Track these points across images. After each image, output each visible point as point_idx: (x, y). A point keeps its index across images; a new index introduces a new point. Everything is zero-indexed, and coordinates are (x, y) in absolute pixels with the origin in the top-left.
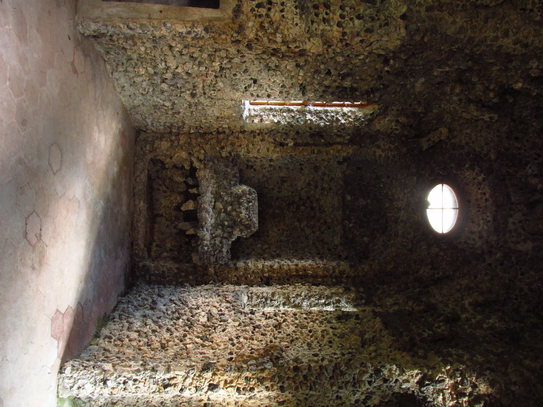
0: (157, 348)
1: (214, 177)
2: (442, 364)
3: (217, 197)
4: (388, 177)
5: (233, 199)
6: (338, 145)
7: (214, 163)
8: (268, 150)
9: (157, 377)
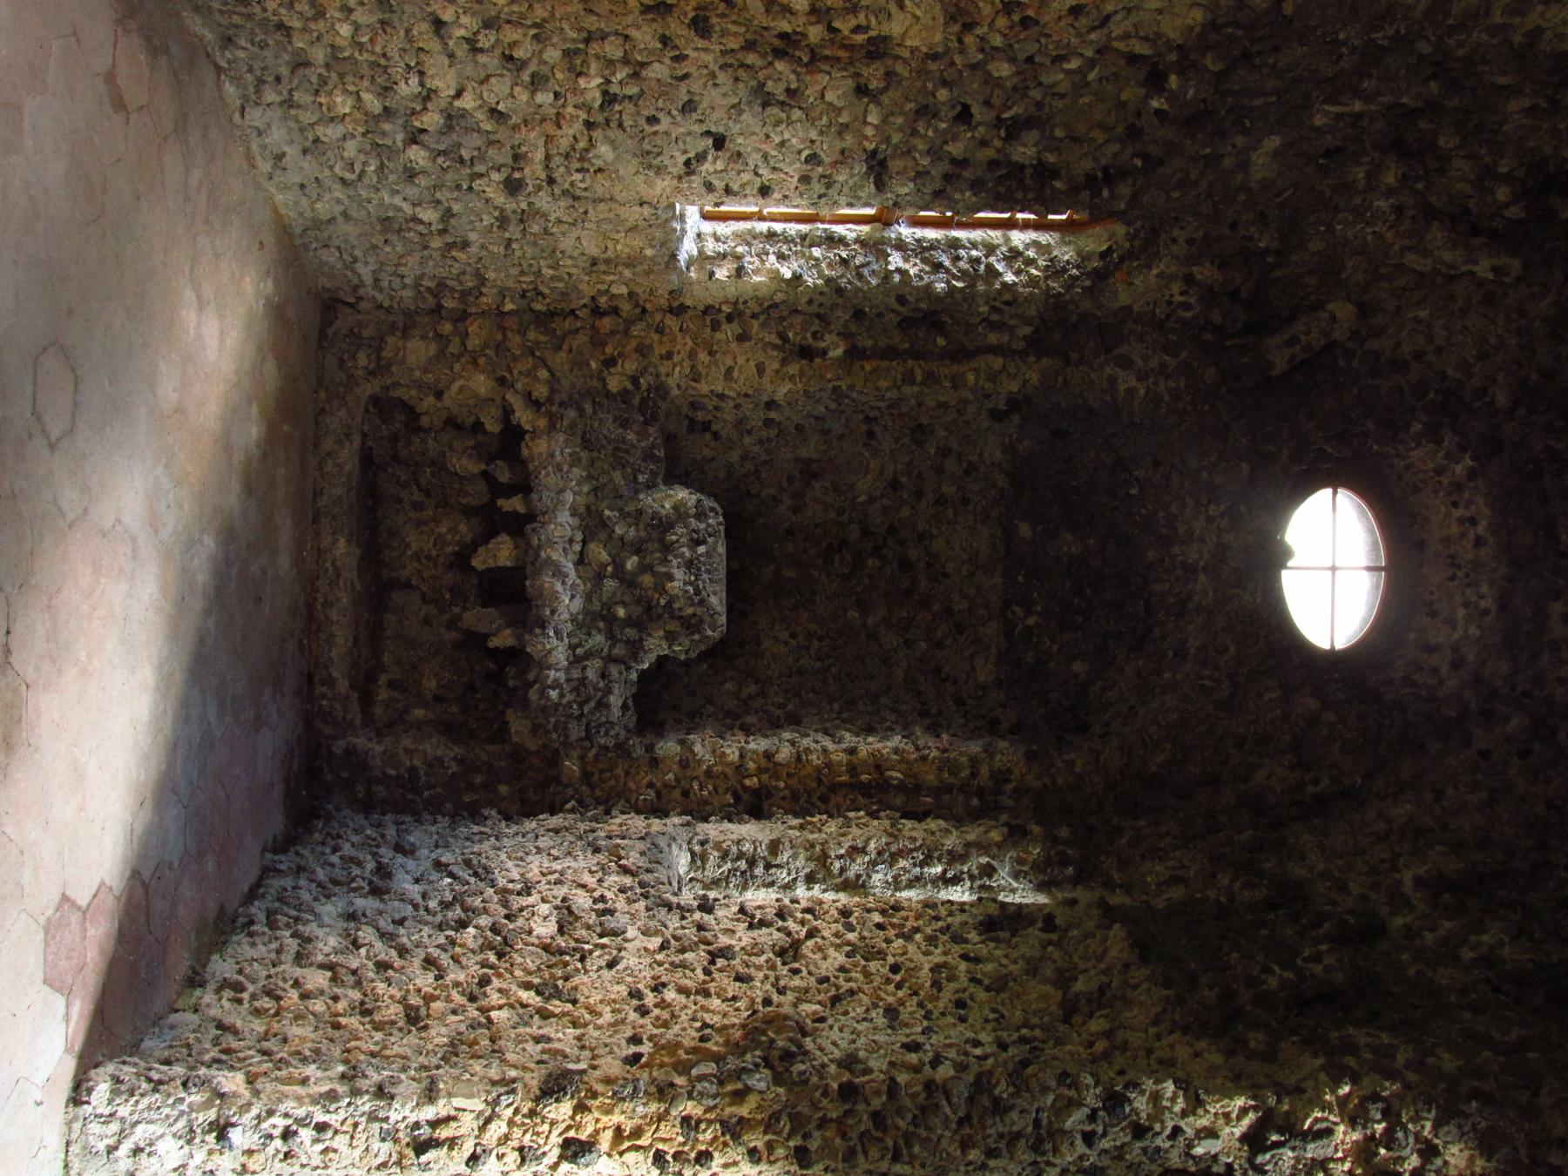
0: (393, 1023)
1: (579, 460)
2: (1323, 1077)
3: (592, 525)
5: (643, 534)
6: (990, 358)
8: (761, 369)
9: (394, 1116)
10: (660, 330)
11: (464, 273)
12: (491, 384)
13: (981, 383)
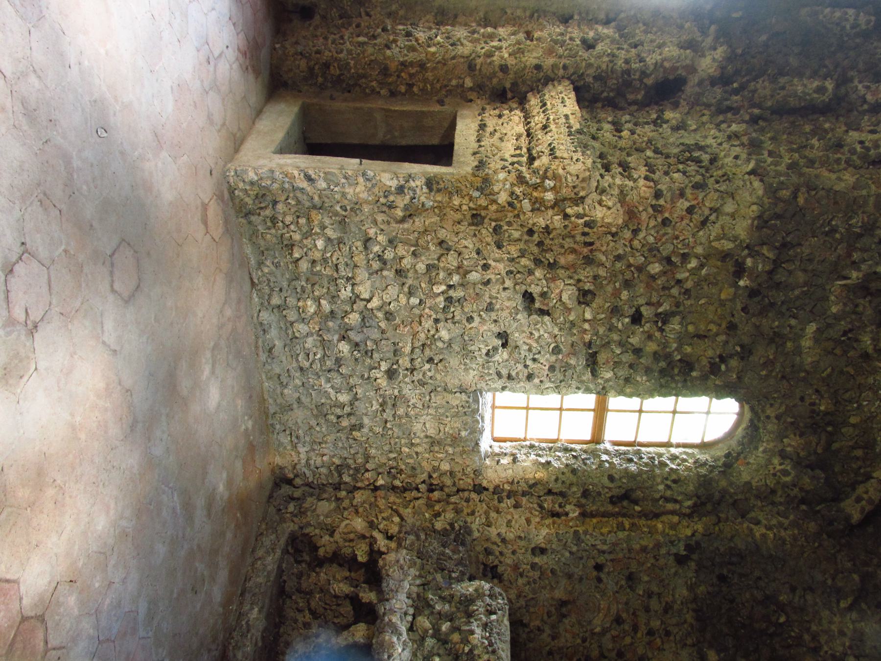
1: (415, 563)
3: (420, 605)
4: (793, 589)
5: (454, 609)
6: (670, 517)
7: (418, 537)
8: (528, 521)
10: (468, 500)
11: (357, 453)
12: (365, 524)
13: (667, 531)
